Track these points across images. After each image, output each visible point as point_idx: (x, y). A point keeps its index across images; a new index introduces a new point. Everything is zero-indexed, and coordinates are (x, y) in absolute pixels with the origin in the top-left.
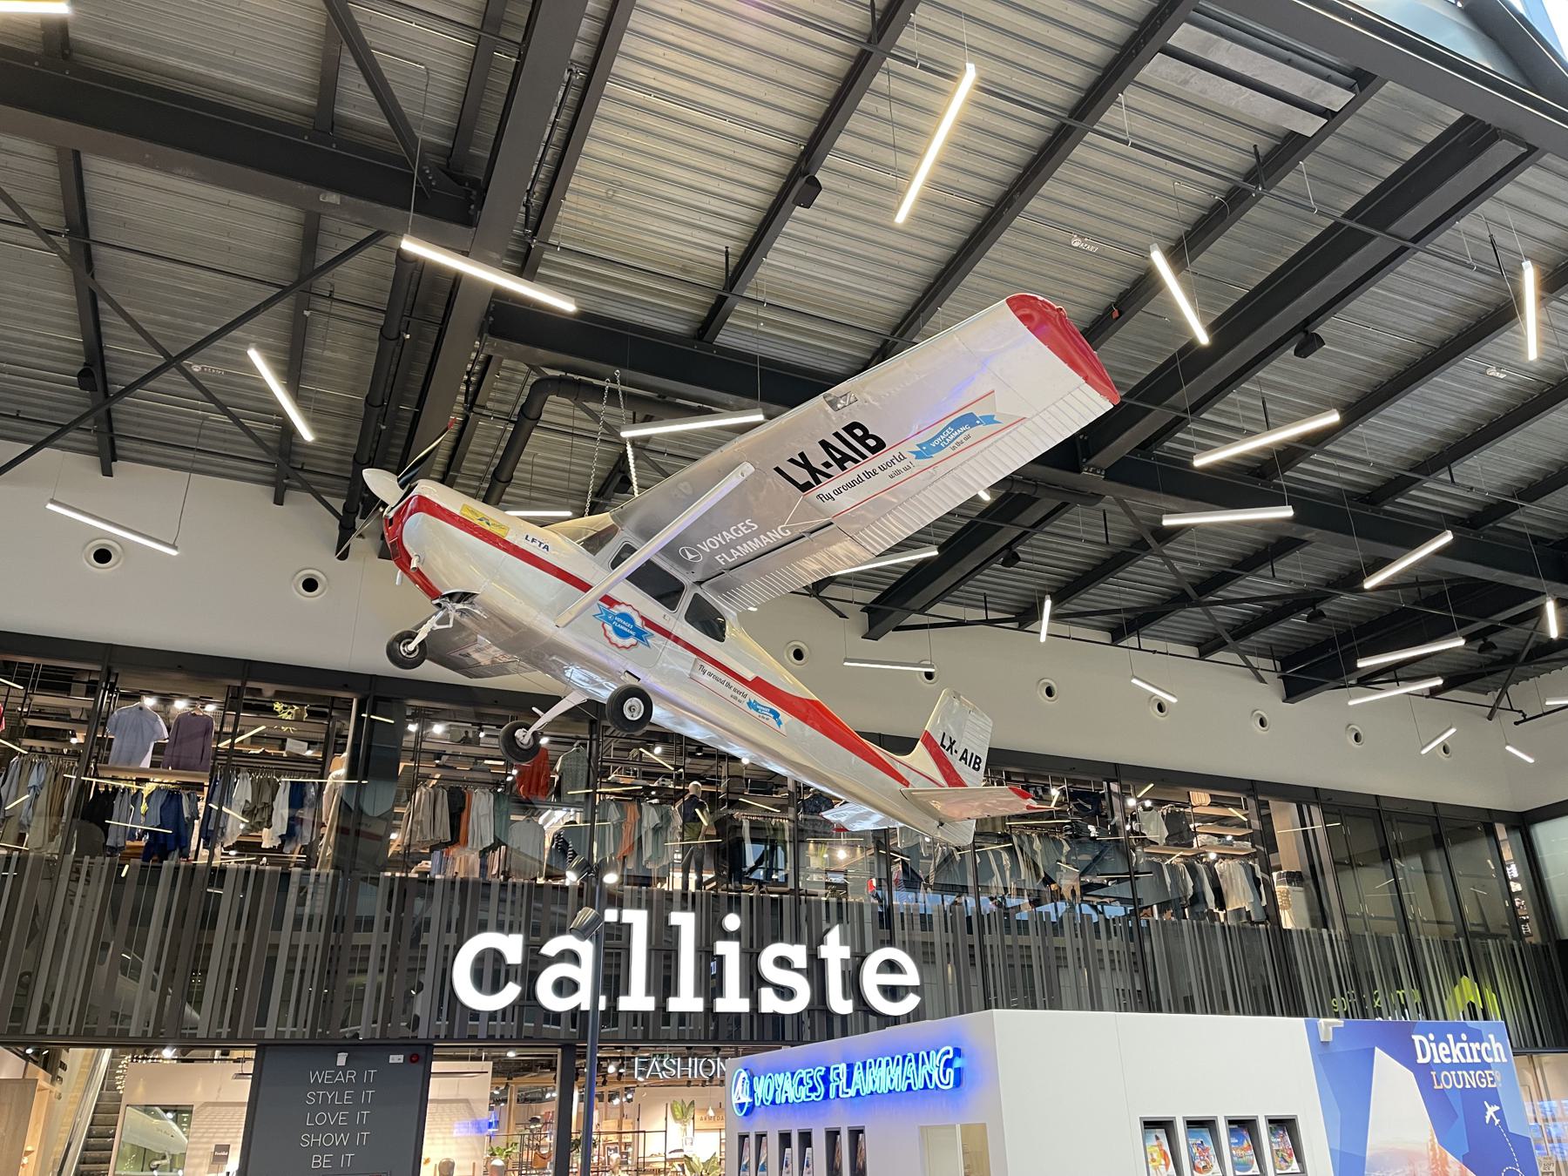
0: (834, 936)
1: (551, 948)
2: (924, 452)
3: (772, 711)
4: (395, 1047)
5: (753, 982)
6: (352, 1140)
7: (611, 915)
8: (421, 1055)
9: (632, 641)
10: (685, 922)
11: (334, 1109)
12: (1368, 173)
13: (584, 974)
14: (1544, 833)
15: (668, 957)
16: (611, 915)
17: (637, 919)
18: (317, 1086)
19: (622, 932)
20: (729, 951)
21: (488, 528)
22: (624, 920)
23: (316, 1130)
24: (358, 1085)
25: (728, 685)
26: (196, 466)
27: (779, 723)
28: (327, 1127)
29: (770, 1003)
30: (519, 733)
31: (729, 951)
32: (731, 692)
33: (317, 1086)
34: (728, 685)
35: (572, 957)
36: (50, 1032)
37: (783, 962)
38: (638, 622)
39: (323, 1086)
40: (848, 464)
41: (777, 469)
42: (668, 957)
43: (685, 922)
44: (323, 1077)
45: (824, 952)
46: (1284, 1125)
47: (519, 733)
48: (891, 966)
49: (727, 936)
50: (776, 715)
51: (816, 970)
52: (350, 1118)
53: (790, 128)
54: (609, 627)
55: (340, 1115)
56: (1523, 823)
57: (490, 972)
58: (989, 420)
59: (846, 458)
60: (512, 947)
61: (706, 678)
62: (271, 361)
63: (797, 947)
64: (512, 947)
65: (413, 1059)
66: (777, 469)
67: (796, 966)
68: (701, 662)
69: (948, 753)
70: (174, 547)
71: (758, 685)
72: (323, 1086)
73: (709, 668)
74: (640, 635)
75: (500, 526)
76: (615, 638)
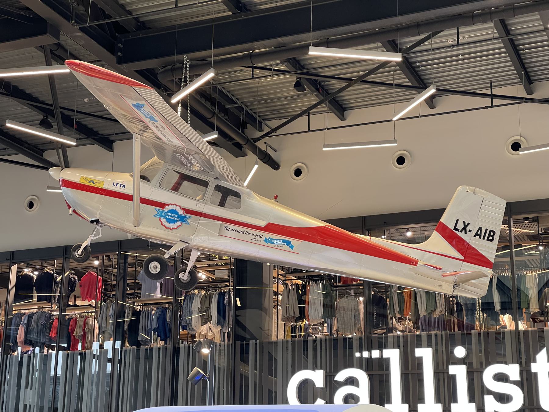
1: (341, 376)
3: (284, 241)
7: (376, 354)
9: (178, 223)
10: (425, 354)
15: (381, 382)
16: (376, 354)
17: (393, 355)
19: (384, 364)
20: (459, 372)
21: (93, 185)
22: (385, 356)
25: (247, 233)
26: (396, 99)
27: (292, 247)
30: (181, 275)
31: (459, 372)
32: (251, 236)
34: (247, 233)
35: (352, 381)
37: (501, 378)
38: (181, 212)
40: (478, 237)
41: (457, 220)
42: (381, 382)
43: (425, 354)
45: (534, 368)
47: (181, 275)
50: (288, 243)
54: (163, 220)
60: (317, 377)
61: (230, 233)
62: (208, 83)
63: (511, 366)
64: (317, 377)
66: (457, 220)
67: (512, 379)
68: (226, 224)
69: (462, 235)
70: (394, 141)
71: (270, 228)
73: (231, 226)
74: (182, 219)
75: (100, 182)
76: (168, 225)
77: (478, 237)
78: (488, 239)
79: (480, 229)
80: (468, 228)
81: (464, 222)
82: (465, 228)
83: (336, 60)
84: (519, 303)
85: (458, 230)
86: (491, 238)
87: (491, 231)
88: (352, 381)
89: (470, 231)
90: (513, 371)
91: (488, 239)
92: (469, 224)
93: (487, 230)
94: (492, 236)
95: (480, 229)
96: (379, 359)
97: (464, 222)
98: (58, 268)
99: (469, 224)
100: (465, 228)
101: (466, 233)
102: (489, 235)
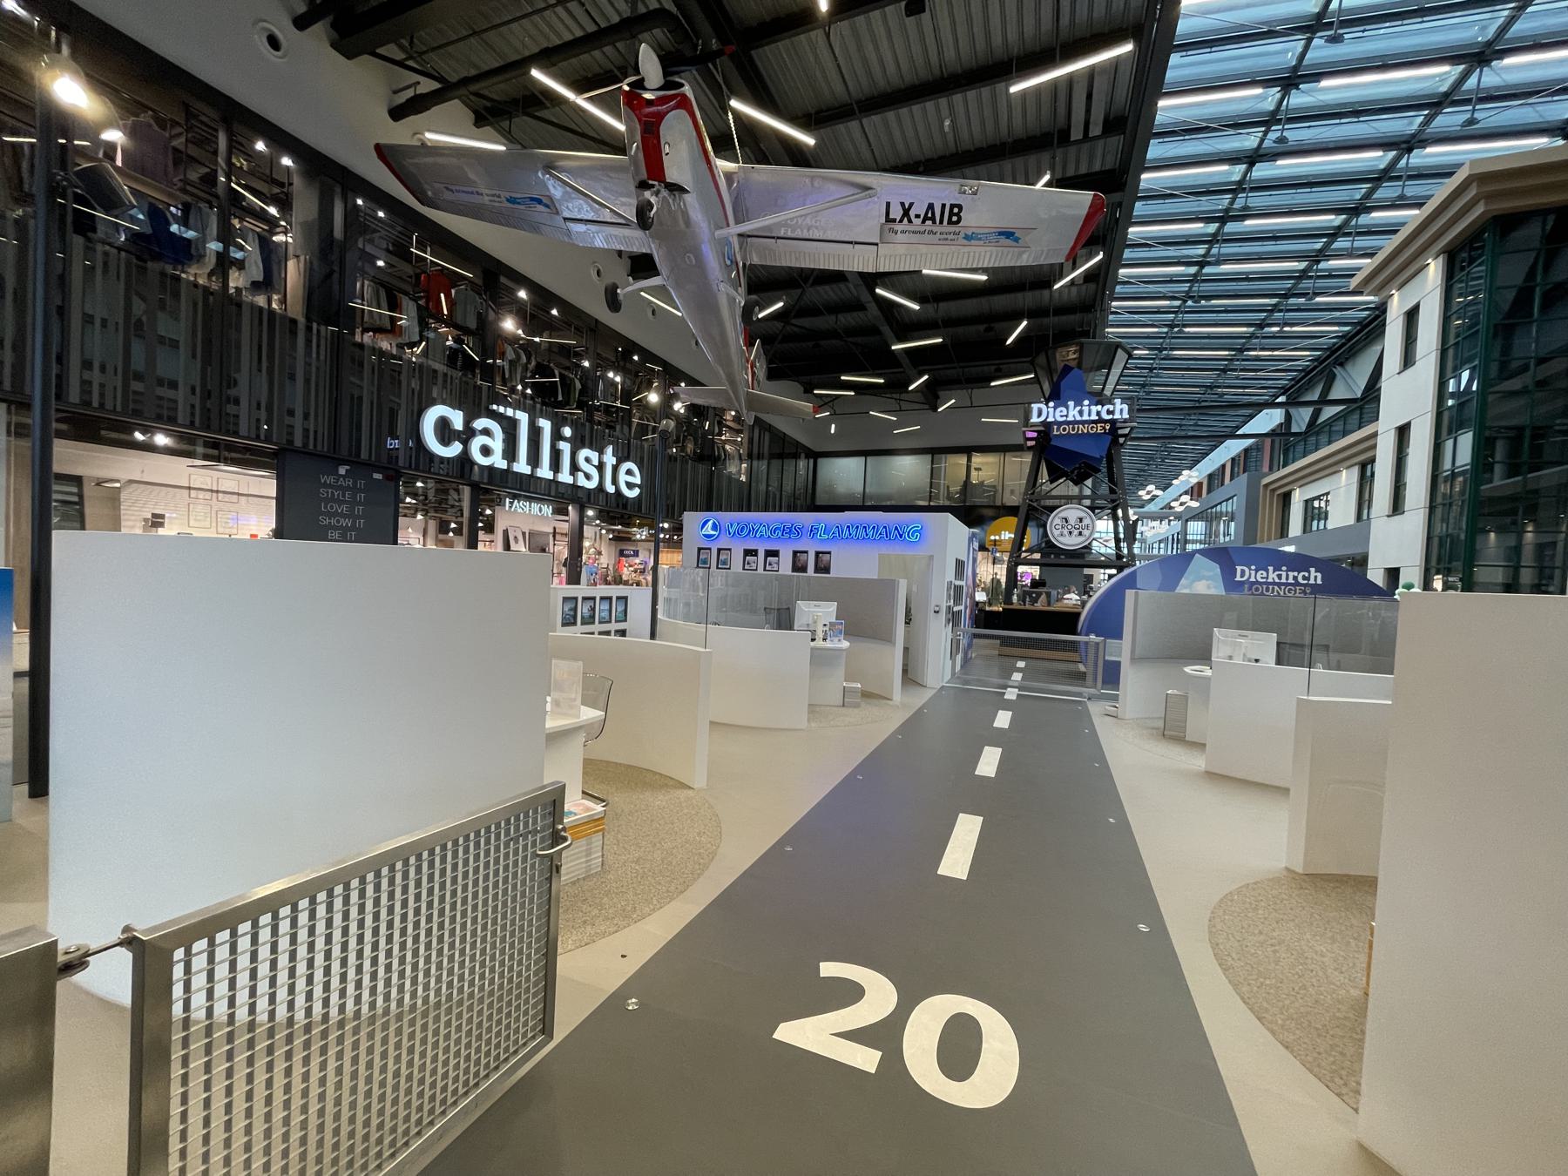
0: (610, 450)
2: (967, 237)
4: (379, 469)
5: (575, 468)
6: (354, 523)
8: (393, 474)
11: (341, 503)
12: (548, 39)
13: (497, 444)
14: (820, 461)
18: (325, 485)
20: (565, 447)
23: (331, 515)
24: (354, 490)
28: (335, 514)
29: (582, 481)
31: (565, 447)
33: (325, 485)
35: (486, 432)
36: (95, 404)
39: (330, 486)
40: (929, 222)
41: (888, 204)
44: (330, 480)
46: (795, 553)
48: (629, 472)
49: (565, 439)
51: (601, 467)
52: (352, 510)
53: (1043, 29)
55: (344, 507)
56: (814, 456)
57: (445, 431)
58: (1017, 240)
59: (933, 219)
60: (457, 419)
64: (457, 419)
65: (387, 478)
66: (888, 204)
72: (330, 486)
77: (929, 222)
78: (950, 222)
79: (931, 207)
80: (912, 214)
81: (903, 204)
82: (906, 213)
83: (107, 85)
84: (381, 377)
85: (894, 220)
86: (955, 219)
87: (952, 206)
88: (486, 432)
89: (918, 216)
90: (594, 456)
91: (950, 222)
92: (911, 205)
93: (944, 206)
94: (958, 215)
95: (931, 207)
96: (103, 426)
97: (903, 204)
98: (359, 314)
99: (911, 205)
100: (906, 213)
101: (910, 221)
102: (951, 214)
